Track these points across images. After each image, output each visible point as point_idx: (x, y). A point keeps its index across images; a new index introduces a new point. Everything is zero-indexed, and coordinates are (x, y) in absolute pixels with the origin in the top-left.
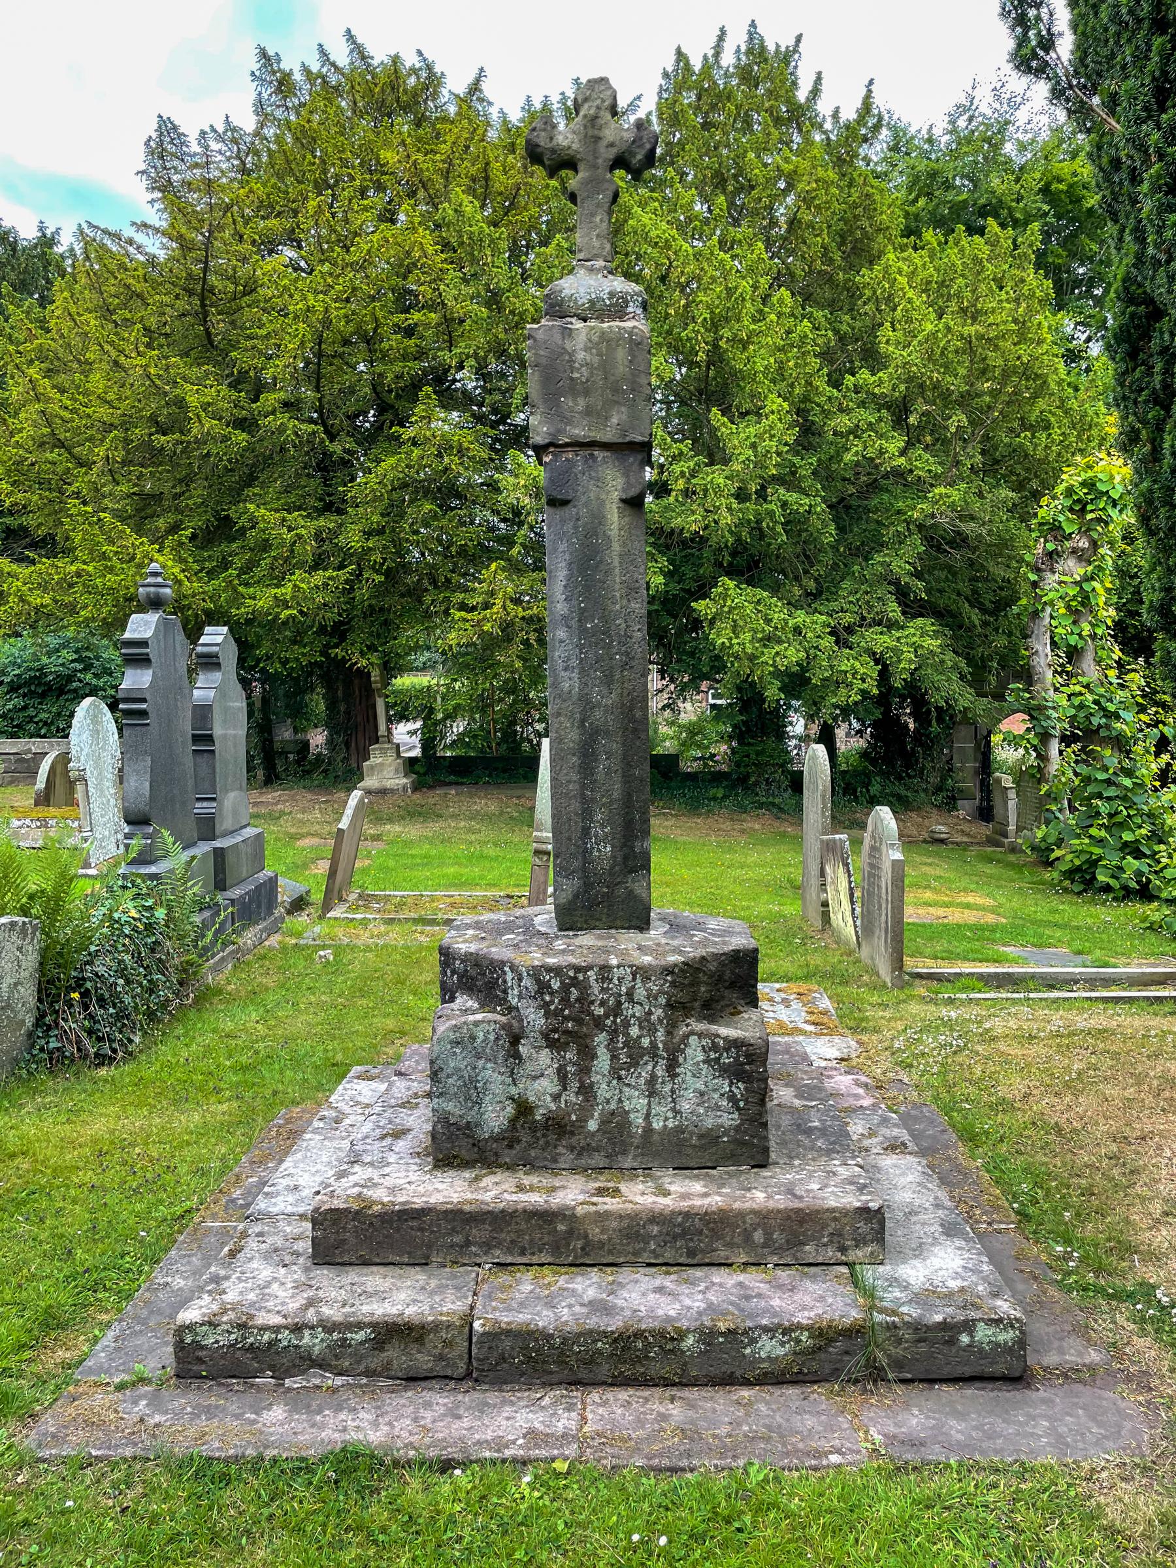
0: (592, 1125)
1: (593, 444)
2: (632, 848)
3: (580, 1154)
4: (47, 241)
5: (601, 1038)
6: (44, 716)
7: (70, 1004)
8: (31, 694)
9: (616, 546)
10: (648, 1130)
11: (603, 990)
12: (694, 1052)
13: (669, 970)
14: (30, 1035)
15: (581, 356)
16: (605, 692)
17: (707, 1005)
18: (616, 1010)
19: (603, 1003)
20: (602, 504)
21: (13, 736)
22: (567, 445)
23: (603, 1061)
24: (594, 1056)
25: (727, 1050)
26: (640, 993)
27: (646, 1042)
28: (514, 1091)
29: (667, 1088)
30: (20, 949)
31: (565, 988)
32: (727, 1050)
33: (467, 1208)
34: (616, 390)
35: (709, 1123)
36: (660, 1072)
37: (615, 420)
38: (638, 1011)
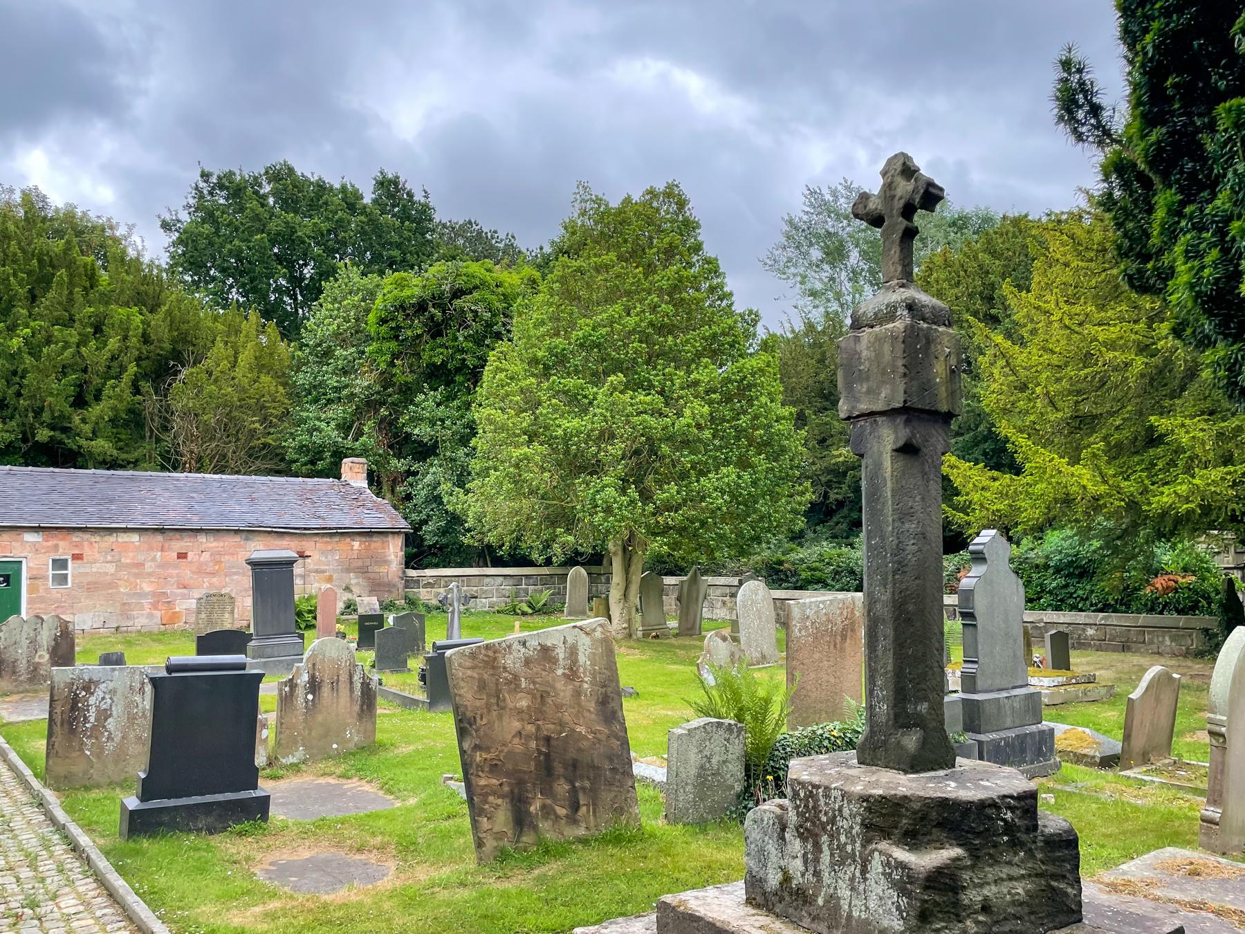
0: (820, 901)
1: (872, 414)
2: (905, 708)
3: (813, 920)
4: (753, 318)
5: (825, 838)
6: (1080, 592)
7: (765, 782)
8: (1069, 576)
9: (889, 484)
10: (850, 916)
11: (826, 804)
12: (876, 865)
13: (865, 799)
14: (738, 796)
15: (865, 353)
16: (883, 590)
17: (906, 834)
18: (833, 821)
19: (826, 814)
20: (880, 454)
21: (1058, 608)
22: (858, 416)
23: (825, 857)
24: (821, 852)
25: (896, 868)
26: (846, 812)
27: (849, 848)
28: (782, 863)
29: (862, 887)
30: (728, 740)
31: (807, 798)
32: (896, 868)
33: (718, 924)
34: (884, 373)
35: (885, 923)
36: (858, 874)
37: (883, 395)
38: (845, 824)
